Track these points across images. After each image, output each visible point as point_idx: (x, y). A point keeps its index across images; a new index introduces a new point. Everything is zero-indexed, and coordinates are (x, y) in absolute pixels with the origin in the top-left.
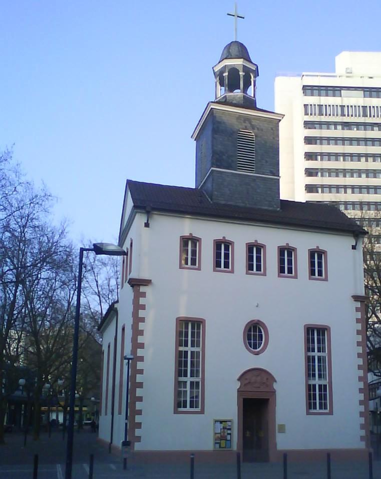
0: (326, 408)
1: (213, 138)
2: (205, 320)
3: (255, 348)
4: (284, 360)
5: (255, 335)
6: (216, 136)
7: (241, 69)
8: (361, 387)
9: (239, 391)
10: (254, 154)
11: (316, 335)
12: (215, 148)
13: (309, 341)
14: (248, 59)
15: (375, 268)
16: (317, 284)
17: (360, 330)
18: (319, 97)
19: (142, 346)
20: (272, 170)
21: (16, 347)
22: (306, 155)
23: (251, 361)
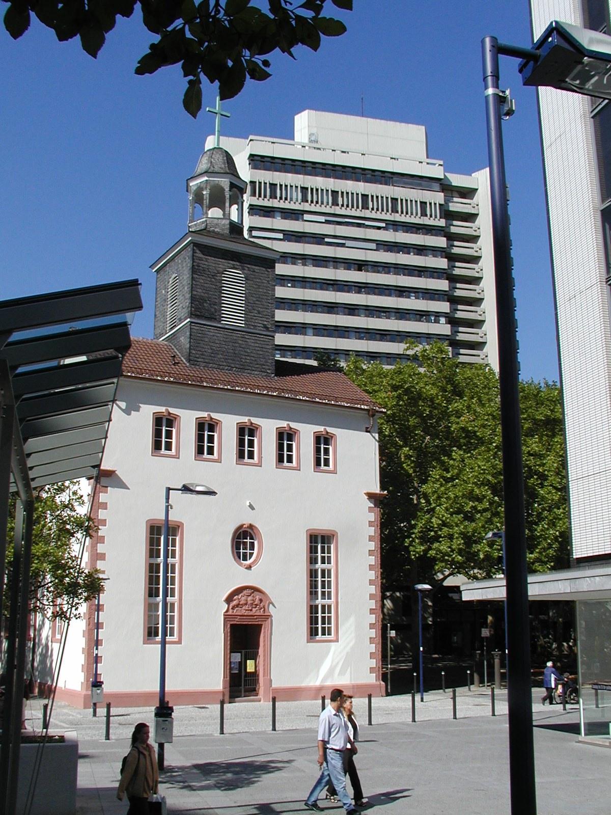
0: (329, 634)
1: (193, 278)
2: (183, 524)
3: (245, 559)
4: (280, 573)
5: (243, 540)
6: (195, 276)
7: (227, 189)
8: (372, 593)
9: (227, 617)
10: (243, 302)
11: (319, 542)
12: (195, 293)
13: (312, 550)
14: (235, 174)
15: (597, 637)
16: (322, 478)
17: (372, 536)
18: (334, 270)
19: (102, 557)
20: (265, 323)
21: (533, 444)
22: (251, 209)
23: (239, 576)
